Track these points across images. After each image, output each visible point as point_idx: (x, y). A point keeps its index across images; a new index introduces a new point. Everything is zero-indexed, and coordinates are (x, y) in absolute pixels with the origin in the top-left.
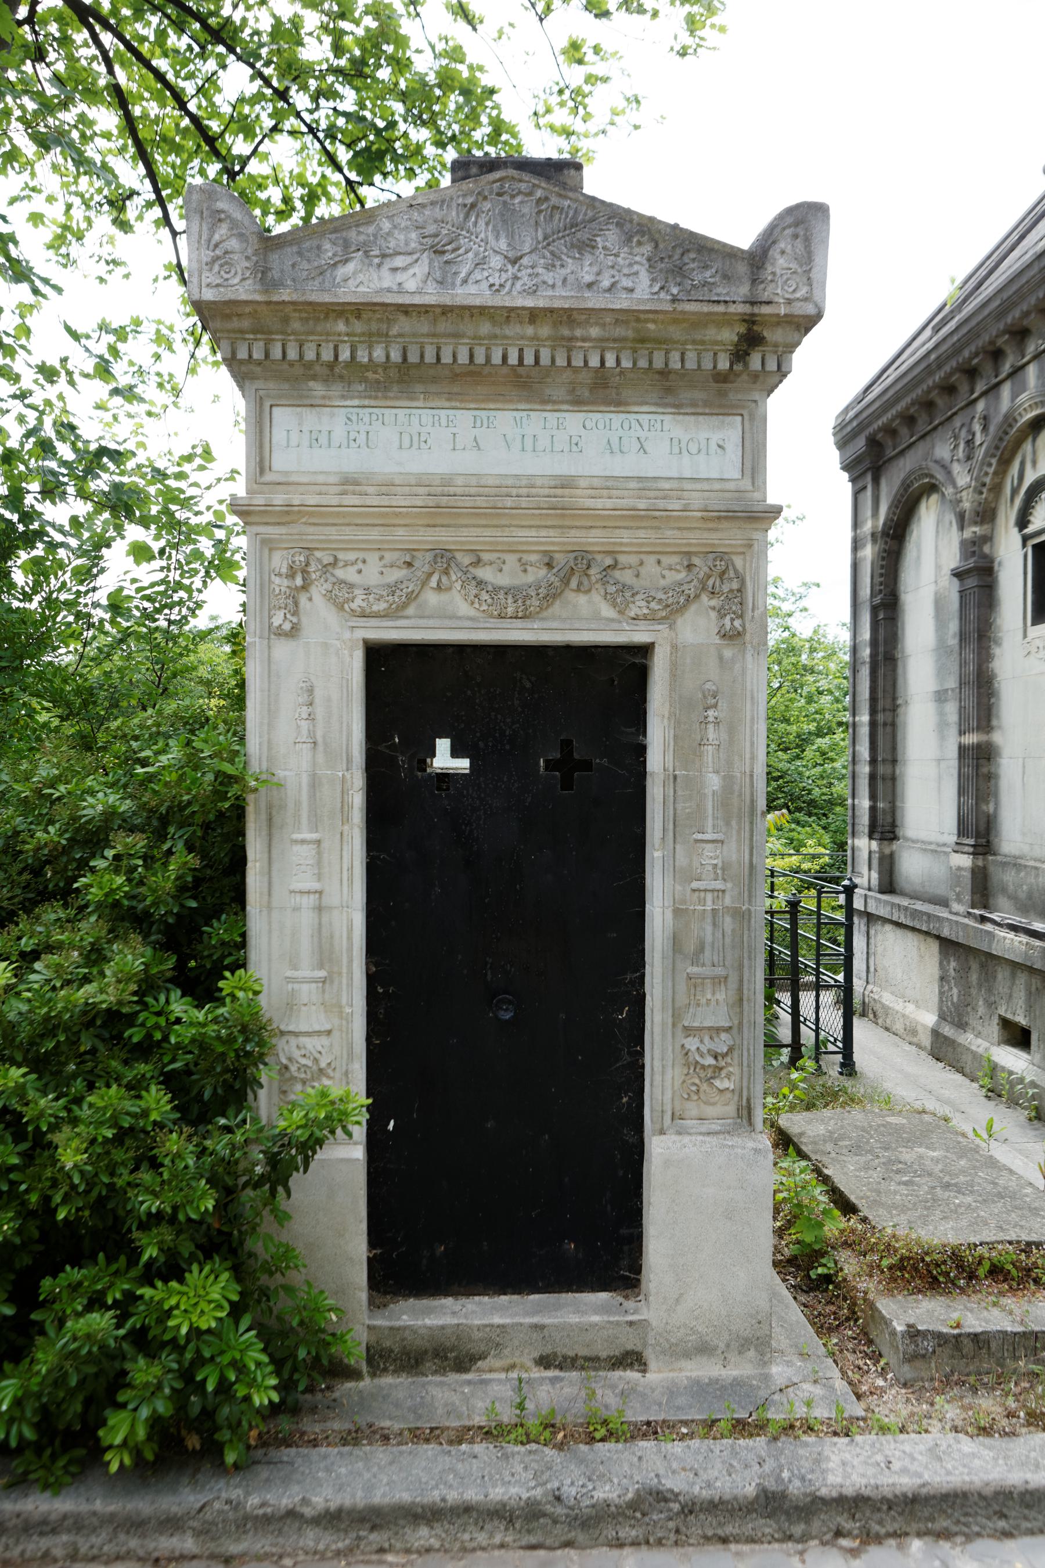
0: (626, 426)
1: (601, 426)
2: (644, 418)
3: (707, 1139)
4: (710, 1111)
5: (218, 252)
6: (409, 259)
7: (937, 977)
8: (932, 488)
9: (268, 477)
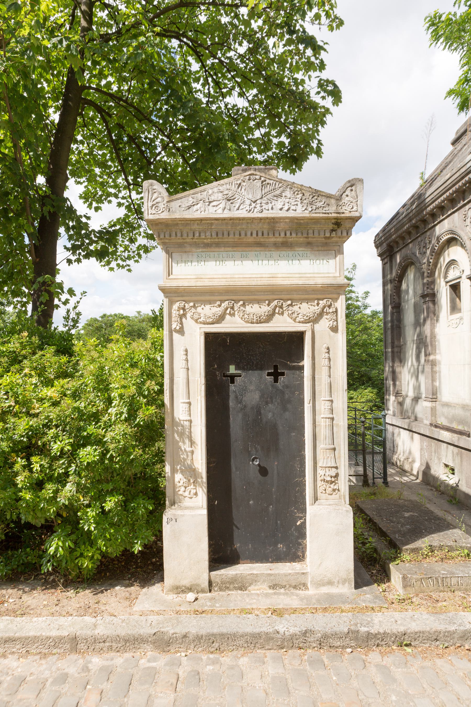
0: (294, 256)
1: (285, 256)
2: (301, 253)
3: (329, 507)
4: (82, 180)
5: (154, 203)
6: (218, 202)
8: (412, 263)
9: (171, 277)
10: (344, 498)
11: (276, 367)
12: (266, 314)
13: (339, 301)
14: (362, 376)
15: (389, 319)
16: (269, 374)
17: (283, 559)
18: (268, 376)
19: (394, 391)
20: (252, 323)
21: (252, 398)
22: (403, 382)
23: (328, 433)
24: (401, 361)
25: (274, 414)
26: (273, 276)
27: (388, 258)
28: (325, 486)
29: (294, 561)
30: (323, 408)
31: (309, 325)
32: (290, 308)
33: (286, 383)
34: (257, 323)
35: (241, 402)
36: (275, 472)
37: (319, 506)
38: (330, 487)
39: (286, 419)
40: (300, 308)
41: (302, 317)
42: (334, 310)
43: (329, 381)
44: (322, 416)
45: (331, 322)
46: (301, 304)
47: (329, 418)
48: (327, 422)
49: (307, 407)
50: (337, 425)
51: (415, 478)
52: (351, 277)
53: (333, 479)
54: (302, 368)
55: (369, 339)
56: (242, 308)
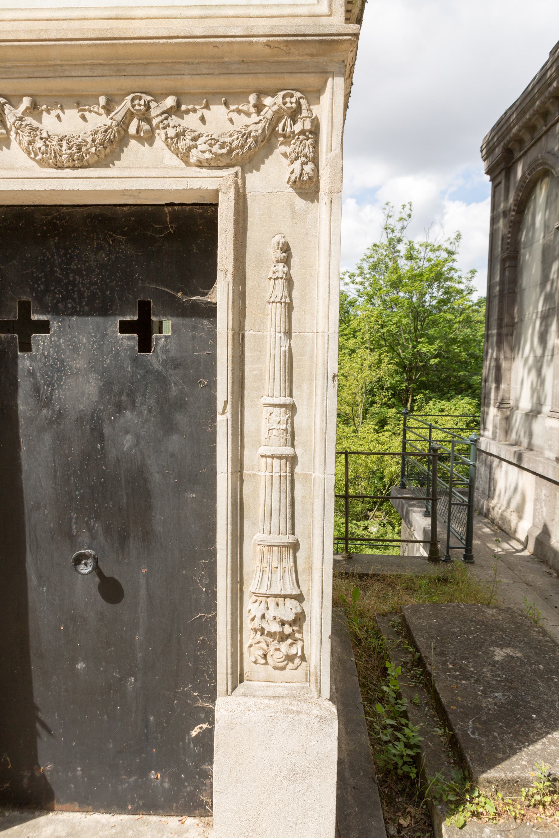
3: (272, 702)
7: (533, 498)
10: (318, 681)
11: (145, 309)
12: (99, 136)
13: (325, 98)
14: (461, 383)
15: (498, 279)
16: (125, 327)
17: (163, 808)
18: (121, 331)
19: (496, 399)
20: (59, 167)
21: (81, 391)
22: (513, 385)
23: (278, 500)
24: (512, 349)
25: (138, 437)
26: (121, 13)
27: (503, 173)
28: (263, 645)
29: (191, 814)
30: (264, 429)
31: (228, 173)
32: (174, 120)
33: (173, 354)
34: (74, 167)
35: (48, 403)
36: (143, 592)
37: (245, 699)
38: (278, 650)
39: (172, 455)
40: (203, 119)
41: (205, 147)
42: (308, 126)
43: (285, 348)
44: (262, 450)
45: (297, 165)
46: (207, 107)
47: (280, 458)
48: (276, 469)
49: (223, 422)
50: (307, 478)
51: (520, 547)
52: (453, 250)
53: (287, 629)
54: (210, 311)
55: (474, 336)
56: (29, 120)
